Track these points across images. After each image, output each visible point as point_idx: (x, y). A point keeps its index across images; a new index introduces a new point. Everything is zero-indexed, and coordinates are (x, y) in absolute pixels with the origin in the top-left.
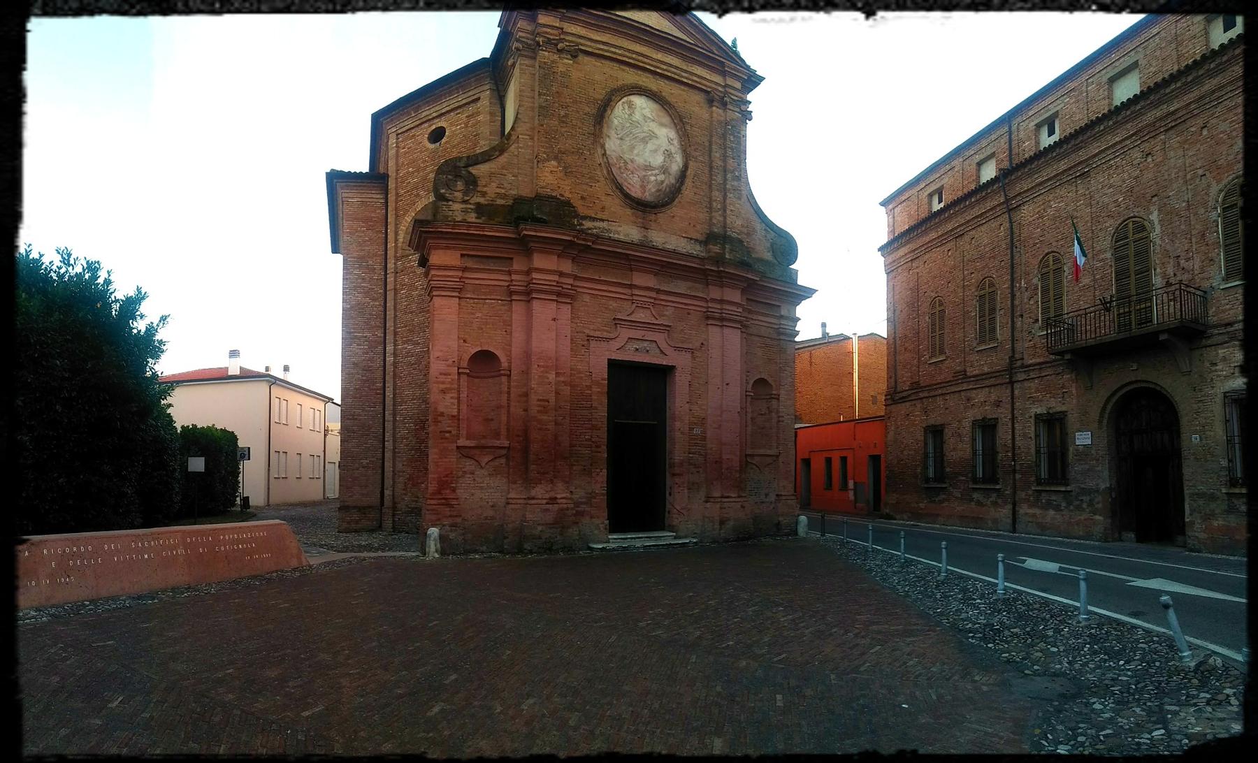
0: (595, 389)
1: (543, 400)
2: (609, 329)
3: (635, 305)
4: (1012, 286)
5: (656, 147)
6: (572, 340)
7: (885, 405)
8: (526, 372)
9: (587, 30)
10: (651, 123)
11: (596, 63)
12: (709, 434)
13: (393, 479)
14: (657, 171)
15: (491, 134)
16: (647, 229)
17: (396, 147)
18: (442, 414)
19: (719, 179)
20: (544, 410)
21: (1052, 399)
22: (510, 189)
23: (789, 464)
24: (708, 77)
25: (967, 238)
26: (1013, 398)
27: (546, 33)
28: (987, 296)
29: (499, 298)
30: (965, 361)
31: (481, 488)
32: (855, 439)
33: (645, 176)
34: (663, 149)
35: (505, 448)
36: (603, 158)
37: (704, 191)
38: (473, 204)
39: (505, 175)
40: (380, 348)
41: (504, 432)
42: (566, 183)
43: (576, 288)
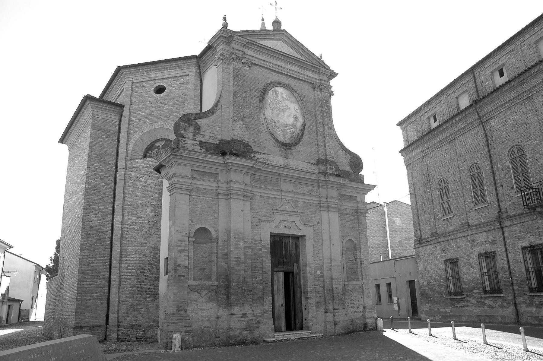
0: (264, 250)
1: (237, 258)
3: (283, 201)
4: (492, 168)
5: (289, 113)
6: (251, 222)
8: (227, 241)
11: (259, 70)
12: (325, 273)
13: (118, 306)
16: (287, 158)
18: (179, 265)
19: (321, 129)
20: (238, 263)
21: (532, 236)
22: (217, 135)
23: (369, 289)
24: (312, 76)
25: (457, 142)
26: (504, 238)
27: (237, 53)
28: (476, 176)
29: (211, 196)
31: (201, 310)
32: (395, 271)
35: (215, 286)
36: (264, 120)
40: (110, 217)
41: (214, 276)
43: (253, 193)
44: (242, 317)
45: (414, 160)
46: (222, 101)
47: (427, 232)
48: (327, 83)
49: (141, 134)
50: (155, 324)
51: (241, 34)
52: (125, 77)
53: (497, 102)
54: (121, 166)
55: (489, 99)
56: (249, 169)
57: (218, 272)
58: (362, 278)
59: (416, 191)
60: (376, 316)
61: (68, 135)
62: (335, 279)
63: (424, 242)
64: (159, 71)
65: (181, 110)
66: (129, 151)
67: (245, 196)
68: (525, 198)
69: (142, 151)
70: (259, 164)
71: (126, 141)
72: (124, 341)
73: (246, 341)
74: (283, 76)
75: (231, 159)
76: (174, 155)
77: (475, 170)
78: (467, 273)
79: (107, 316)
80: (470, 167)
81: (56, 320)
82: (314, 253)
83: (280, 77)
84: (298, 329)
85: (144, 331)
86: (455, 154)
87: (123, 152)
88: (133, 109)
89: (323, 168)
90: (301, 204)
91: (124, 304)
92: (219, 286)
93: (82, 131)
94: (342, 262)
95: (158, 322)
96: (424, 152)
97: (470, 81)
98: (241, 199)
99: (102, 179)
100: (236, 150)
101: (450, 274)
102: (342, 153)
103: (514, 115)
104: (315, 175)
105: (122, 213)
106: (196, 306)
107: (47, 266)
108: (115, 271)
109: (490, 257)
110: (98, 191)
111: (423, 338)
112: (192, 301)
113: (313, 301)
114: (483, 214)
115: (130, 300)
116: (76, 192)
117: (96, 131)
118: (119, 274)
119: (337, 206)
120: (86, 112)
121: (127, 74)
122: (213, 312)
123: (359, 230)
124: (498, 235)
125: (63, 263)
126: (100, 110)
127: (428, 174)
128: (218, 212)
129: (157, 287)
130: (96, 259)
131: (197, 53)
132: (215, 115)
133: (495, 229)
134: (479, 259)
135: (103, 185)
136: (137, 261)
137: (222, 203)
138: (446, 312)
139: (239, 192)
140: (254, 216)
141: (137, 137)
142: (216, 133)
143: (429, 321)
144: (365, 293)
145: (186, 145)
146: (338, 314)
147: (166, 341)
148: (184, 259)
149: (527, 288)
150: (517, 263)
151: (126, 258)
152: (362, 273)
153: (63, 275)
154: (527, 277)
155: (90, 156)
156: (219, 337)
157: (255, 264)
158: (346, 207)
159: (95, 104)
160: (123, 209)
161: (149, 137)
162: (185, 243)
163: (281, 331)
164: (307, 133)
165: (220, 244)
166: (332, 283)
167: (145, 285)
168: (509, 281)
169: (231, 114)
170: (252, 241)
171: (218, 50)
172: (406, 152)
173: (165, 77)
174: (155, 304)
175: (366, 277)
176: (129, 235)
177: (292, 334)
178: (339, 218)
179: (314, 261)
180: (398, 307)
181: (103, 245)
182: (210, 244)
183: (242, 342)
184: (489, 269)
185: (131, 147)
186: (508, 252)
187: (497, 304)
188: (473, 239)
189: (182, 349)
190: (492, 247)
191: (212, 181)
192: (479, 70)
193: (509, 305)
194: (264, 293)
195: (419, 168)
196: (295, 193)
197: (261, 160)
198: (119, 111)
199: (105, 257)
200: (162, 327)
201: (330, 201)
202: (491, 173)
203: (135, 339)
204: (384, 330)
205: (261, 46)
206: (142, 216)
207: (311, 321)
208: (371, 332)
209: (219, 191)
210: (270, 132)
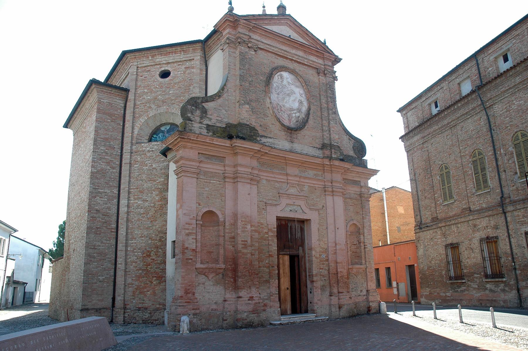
0: (270, 234)
2: (275, 199)
3: (289, 185)
4: (495, 154)
5: (294, 98)
6: (258, 206)
8: (234, 224)
10: (292, 86)
12: (330, 257)
13: (125, 289)
14: (296, 111)
17: (136, 74)
18: (187, 248)
19: (325, 114)
20: (245, 246)
22: (224, 118)
24: (316, 61)
25: (459, 127)
26: (507, 222)
27: (243, 37)
28: (478, 162)
29: (218, 180)
30: (468, 202)
31: (209, 292)
32: (395, 256)
33: (290, 114)
34: (298, 100)
36: (270, 105)
37: (318, 121)
38: (205, 124)
39: (221, 110)
40: (116, 201)
41: (221, 259)
42: (253, 117)
43: (259, 176)
44: (249, 300)
45: (415, 146)
46: (229, 85)
47: (427, 217)
48: (331, 69)
49: (146, 119)
50: (161, 306)
51: (247, 18)
52: (130, 61)
54: (126, 150)
55: (493, 84)
56: (256, 153)
57: (225, 255)
58: (366, 261)
61: (73, 119)
62: (339, 263)
63: (424, 227)
64: (164, 56)
66: (135, 135)
69: (148, 135)
71: (131, 125)
72: (130, 323)
73: (253, 323)
74: (288, 61)
75: (238, 143)
76: (181, 138)
77: (477, 156)
79: (114, 299)
80: (471, 153)
81: (62, 302)
82: (319, 236)
83: (285, 61)
84: (303, 312)
85: (150, 313)
86: (457, 139)
87: (129, 136)
89: (327, 152)
90: (306, 188)
92: (226, 269)
93: (87, 115)
94: (346, 246)
95: (164, 305)
96: (425, 138)
97: (473, 67)
98: (248, 183)
99: (108, 163)
100: (242, 134)
101: (450, 258)
102: (346, 138)
103: (519, 100)
104: (320, 160)
106: (203, 289)
110: (104, 174)
111: (428, 321)
112: (199, 284)
113: (318, 284)
116: (81, 176)
117: (101, 115)
118: (126, 257)
119: (341, 190)
120: (92, 96)
121: (132, 58)
123: (363, 214)
124: (501, 220)
126: (105, 94)
128: (225, 195)
129: (164, 270)
130: (102, 243)
131: (202, 37)
132: (221, 99)
133: (497, 214)
135: (108, 169)
136: (143, 245)
137: (229, 187)
138: (446, 296)
139: (246, 175)
140: (261, 199)
142: (223, 117)
144: (369, 277)
145: (193, 128)
151: (132, 242)
152: (365, 257)
153: (69, 258)
155: (95, 140)
156: (226, 320)
157: (261, 247)
158: (349, 191)
159: (100, 88)
160: (129, 193)
161: (155, 121)
162: (193, 226)
164: (312, 117)
165: (227, 227)
166: (337, 267)
167: (151, 268)
168: (512, 266)
169: (238, 98)
170: (259, 224)
171: (224, 34)
172: (406, 138)
173: (170, 61)
174: (161, 287)
175: (370, 261)
177: (298, 317)
178: (344, 202)
180: (398, 291)
181: (109, 229)
182: (216, 227)
183: (249, 325)
184: (491, 253)
185: (136, 132)
186: (511, 237)
187: (499, 289)
189: (190, 332)
190: (494, 232)
191: (219, 164)
192: (483, 56)
193: (511, 289)
195: (420, 154)
196: (300, 177)
197: (267, 144)
199: (112, 241)
200: (170, 309)
202: (494, 159)
203: (141, 322)
209: (226, 174)
210: (276, 116)
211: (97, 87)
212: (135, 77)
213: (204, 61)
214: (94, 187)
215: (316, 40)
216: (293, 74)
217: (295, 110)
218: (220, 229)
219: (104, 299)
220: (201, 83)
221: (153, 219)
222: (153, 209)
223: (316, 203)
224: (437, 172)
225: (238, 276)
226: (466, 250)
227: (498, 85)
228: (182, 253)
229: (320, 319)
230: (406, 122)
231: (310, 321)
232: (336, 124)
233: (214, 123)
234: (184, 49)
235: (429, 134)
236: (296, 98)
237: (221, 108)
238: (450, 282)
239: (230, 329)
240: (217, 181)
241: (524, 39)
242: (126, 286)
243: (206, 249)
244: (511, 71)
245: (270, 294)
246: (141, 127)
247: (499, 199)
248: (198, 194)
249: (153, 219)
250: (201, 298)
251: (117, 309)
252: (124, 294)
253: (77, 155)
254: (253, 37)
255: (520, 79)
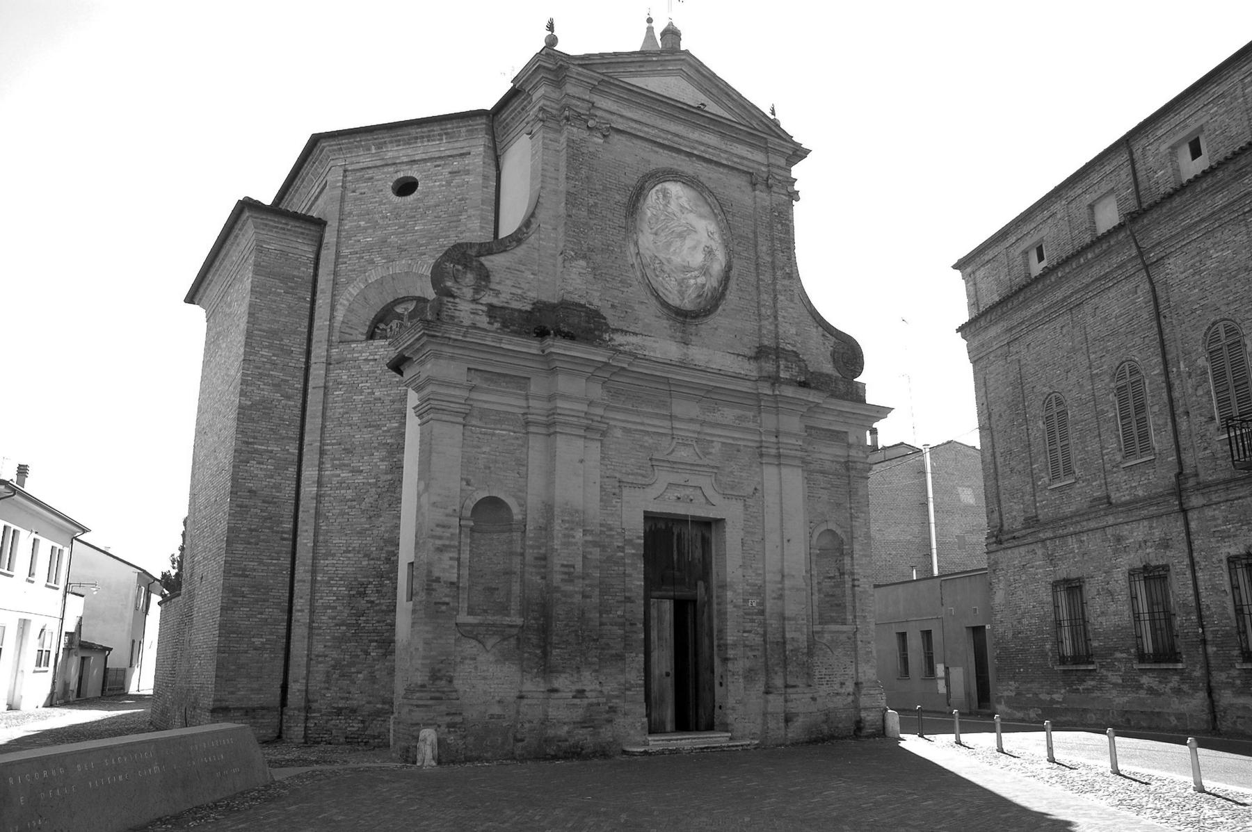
2: (644, 472)
3: (675, 441)
4: (1166, 372)
6: (601, 487)
7: (987, 553)
8: (546, 529)
9: (619, 105)
12: (768, 605)
13: (308, 666)
14: (696, 272)
15: (483, 202)
16: (687, 345)
17: (342, 187)
18: (438, 580)
19: (767, 278)
20: (570, 578)
22: (529, 290)
23: (869, 643)
24: (750, 156)
25: (1088, 308)
26: (1188, 534)
27: (577, 106)
28: (1130, 390)
29: (511, 428)
30: (1106, 483)
31: (485, 678)
32: (942, 605)
35: (515, 626)
36: (637, 258)
40: (292, 470)
41: (515, 606)
42: (595, 287)
43: (607, 421)
44: (574, 697)
45: (990, 350)
46: (542, 215)
47: (1014, 514)
48: (782, 172)
50: (387, 707)
51: (587, 62)
53: (1182, 217)
58: (855, 617)
59: (993, 420)
60: (883, 704)
61: (205, 285)
62: (789, 619)
63: (1008, 539)
64: (404, 145)
65: (452, 234)
66: (337, 325)
67: (588, 428)
68: (1243, 442)
70: (621, 357)
72: (319, 743)
73: (582, 749)
75: (558, 347)
78: (1103, 613)
80: (1115, 368)
82: (744, 558)
83: (674, 158)
85: (363, 722)
87: (324, 325)
88: (345, 230)
89: (769, 367)
90: (716, 449)
91: (320, 663)
94: (809, 581)
95: (391, 703)
96: (1014, 332)
97: (1122, 167)
99: (277, 386)
101: (1064, 614)
102: (815, 332)
104: (749, 384)
105: (320, 461)
106: (473, 670)
107: (164, 575)
108: (301, 589)
109: (1154, 578)
112: (464, 658)
113: (739, 666)
114: (1143, 479)
115: (335, 654)
116: (220, 413)
119: (799, 454)
120: (243, 235)
121: (334, 150)
122: (511, 683)
123: (851, 508)
125: (193, 568)
126: (272, 231)
127: (1020, 383)
129: (393, 625)
130: (261, 563)
131: (489, 106)
132: (524, 246)
133: (1168, 514)
134: (1130, 582)
135: (278, 400)
136: (351, 569)
137: (536, 445)
138: (1052, 701)
139: (575, 419)
141: (353, 292)
142: (526, 286)
143: (999, 720)
144: (861, 652)
145: (457, 313)
146: (795, 696)
147: (404, 744)
148: (448, 567)
149: (1236, 652)
150: (1216, 593)
151: (327, 562)
153: (191, 596)
154: (1238, 626)
155: (249, 335)
156: (522, 740)
158: (818, 456)
159: (262, 219)
160: (322, 453)
161: (381, 293)
162: (451, 530)
163: (664, 732)
164: (735, 287)
167: (367, 622)
168: (1197, 635)
169: (561, 245)
170: (602, 529)
171: (534, 99)
175: (865, 617)
176: (334, 511)
177: (688, 739)
178: (806, 481)
179: (744, 576)
180: (947, 686)
181: (277, 532)
182: (507, 534)
183: (574, 753)
185: (340, 315)
186: (1197, 568)
187: (1168, 687)
188: (1119, 535)
189: (439, 763)
191: (515, 394)
192: (1144, 142)
193: (1195, 689)
194: (627, 641)
195: (1001, 369)
196: (703, 423)
197: (627, 348)
198: (315, 234)
201: (785, 441)
202: (1164, 384)
203: (342, 740)
204: (901, 736)
205: (631, 88)
206: (361, 468)
207: (732, 711)
208: (872, 740)
209: (529, 416)
210: (649, 285)
211: (256, 215)
212: (338, 192)
213: (493, 157)
214: (244, 439)
215: (749, 108)
216: (692, 187)
217: (695, 270)
218: (515, 538)
219: (264, 689)
220: (484, 207)
221: (373, 514)
222: (374, 490)
223: (739, 483)
224: (1038, 412)
225: (551, 643)
226: (1099, 594)
227: (1175, 212)
228: (427, 589)
229: (738, 744)
230: (973, 293)
231: (714, 748)
232: (792, 301)
233: (505, 300)
234: (449, 131)
235: (1022, 323)
236: (699, 242)
237: (523, 268)
238: (1062, 668)
239: (529, 759)
240: (510, 431)
241: (1235, 104)
242: (311, 659)
243: (483, 581)
244: (1204, 179)
245: (624, 685)
246: (351, 306)
247: (1174, 479)
248: (465, 460)
249: (373, 514)
250: (468, 690)
251: (291, 709)
252: (307, 678)
253: (212, 365)
254: (599, 106)
255: (1224, 200)
